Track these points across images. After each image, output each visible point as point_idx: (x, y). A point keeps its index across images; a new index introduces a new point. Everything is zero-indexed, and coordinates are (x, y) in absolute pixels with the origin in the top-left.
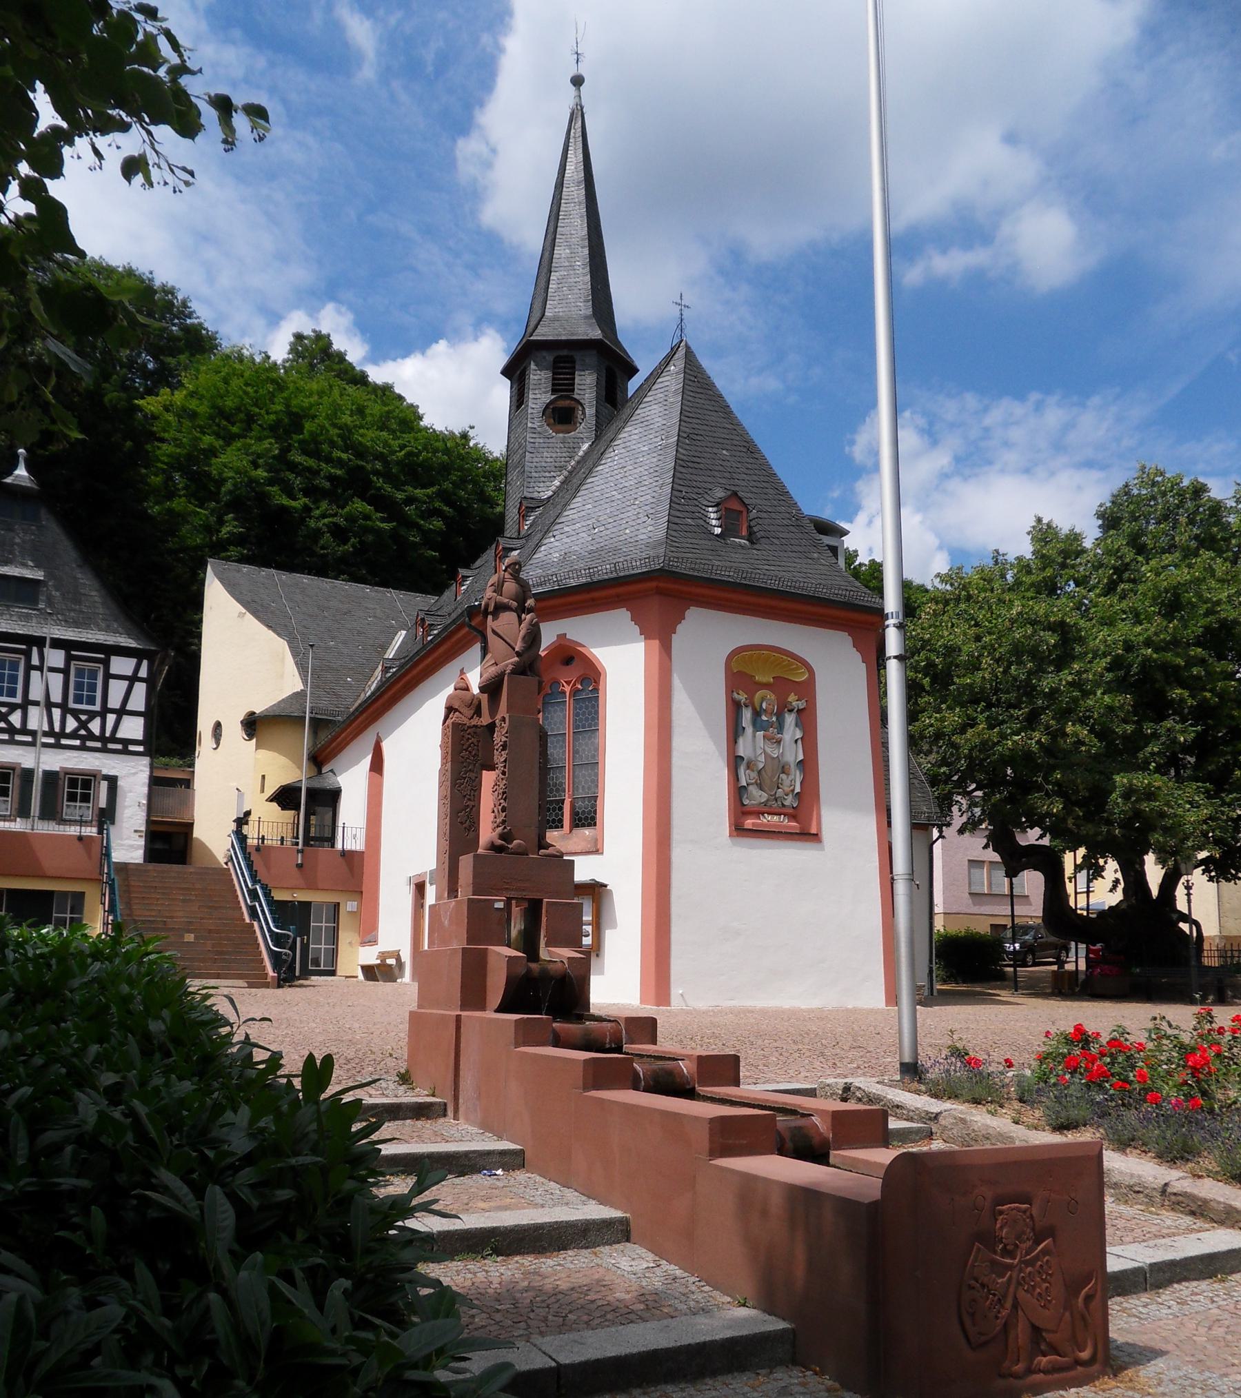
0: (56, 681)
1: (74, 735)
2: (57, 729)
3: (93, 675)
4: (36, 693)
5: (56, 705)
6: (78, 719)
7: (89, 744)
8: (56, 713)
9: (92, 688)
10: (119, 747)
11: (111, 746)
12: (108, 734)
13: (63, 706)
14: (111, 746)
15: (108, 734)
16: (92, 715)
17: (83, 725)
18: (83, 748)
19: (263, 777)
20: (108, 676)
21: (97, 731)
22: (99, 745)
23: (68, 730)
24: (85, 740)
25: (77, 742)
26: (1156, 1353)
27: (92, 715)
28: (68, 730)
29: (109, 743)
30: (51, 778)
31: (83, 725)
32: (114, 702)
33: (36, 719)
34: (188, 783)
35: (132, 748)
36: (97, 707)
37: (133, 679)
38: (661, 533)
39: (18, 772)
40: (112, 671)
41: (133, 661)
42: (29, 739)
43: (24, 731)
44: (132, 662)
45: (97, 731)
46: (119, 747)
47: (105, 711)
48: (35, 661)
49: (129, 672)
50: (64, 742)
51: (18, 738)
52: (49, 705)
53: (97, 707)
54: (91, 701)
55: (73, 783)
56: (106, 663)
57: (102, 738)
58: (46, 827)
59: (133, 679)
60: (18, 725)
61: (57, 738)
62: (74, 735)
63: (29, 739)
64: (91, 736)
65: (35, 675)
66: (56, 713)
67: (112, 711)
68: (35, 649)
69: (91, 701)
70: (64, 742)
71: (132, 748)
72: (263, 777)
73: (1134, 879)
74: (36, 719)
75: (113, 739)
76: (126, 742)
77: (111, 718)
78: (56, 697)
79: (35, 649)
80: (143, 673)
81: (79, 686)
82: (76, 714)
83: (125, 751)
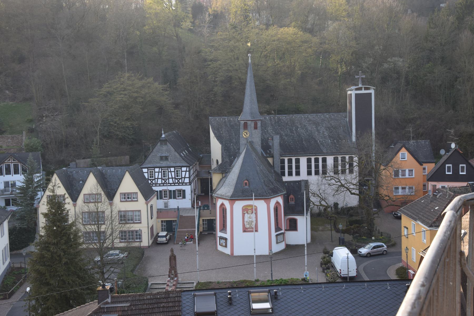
0: (173, 173)
1: (177, 183)
4: (170, 176)
9: (153, 174)
13: (175, 179)
17: (178, 181)
18: (179, 185)
20: (182, 171)
24: (179, 184)
26: (153, 225)
29: (183, 184)
31: (178, 181)
32: (156, 177)
33: (171, 181)
37: (186, 171)
47: (182, 178)
52: (172, 178)
54: (153, 177)
55: (165, 192)
57: (182, 183)
58: (465, 244)
59: (186, 171)
61: (174, 184)
62: (177, 183)
64: (180, 183)
65: (170, 173)
66: (174, 179)
73: (29, 181)
75: (184, 183)
76: (186, 183)
77: (183, 179)
78: (173, 177)
80: (188, 170)
81: (150, 175)
82: (177, 179)
83: (186, 185)
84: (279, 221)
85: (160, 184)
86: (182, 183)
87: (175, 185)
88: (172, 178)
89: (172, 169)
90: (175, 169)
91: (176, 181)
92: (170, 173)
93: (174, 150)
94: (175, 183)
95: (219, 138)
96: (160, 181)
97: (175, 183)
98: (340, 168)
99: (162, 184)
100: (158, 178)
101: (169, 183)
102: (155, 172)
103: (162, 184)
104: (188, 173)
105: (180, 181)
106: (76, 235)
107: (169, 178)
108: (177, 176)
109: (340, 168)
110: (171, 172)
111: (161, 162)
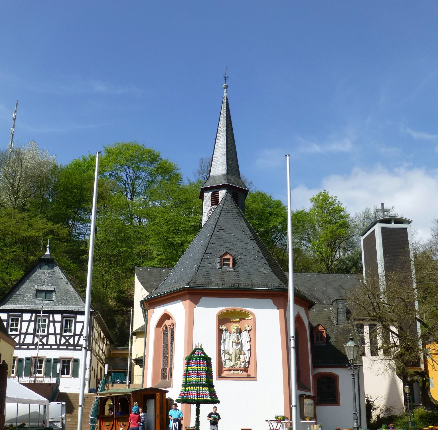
0: (58, 325)
1: (64, 345)
2: (58, 343)
3: (17, 320)
4: (52, 331)
5: (58, 334)
6: (65, 339)
7: (69, 348)
8: (58, 337)
10: (49, 347)
11: (77, 348)
12: (76, 343)
13: (61, 335)
14: (77, 348)
15: (76, 343)
16: (43, 336)
17: (67, 341)
18: (67, 349)
19: (137, 354)
20: (22, 321)
21: (72, 342)
22: (72, 348)
23: (62, 343)
24: (67, 346)
25: (65, 347)
27: (70, 337)
28: (62, 343)
29: (76, 347)
30: (28, 360)
31: (67, 341)
32: (24, 331)
33: (52, 340)
34: (362, 366)
35: (53, 347)
36: (72, 334)
38: (225, 172)
39: (45, 359)
40: (77, 320)
41: (30, 315)
42: (80, 348)
43: (47, 344)
44: (29, 315)
45: (72, 342)
46: (26, 347)
47: (21, 333)
48: (51, 319)
49: (28, 319)
50: (61, 347)
51: (45, 347)
53: (72, 334)
54: (70, 331)
56: (21, 316)
57: (19, 344)
59: (30, 321)
60: (45, 343)
61: (58, 346)
62: (64, 345)
63: (80, 348)
64: (70, 345)
66: (58, 337)
67: (77, 335)
68: (51, 315)
69: (16, 330)
70: (61, 347)
71: (53, 347)
72: (137, 354)
74: (52, 340)
78: (58, 331)
79: (51, 315)
80: (33, 319)
82: (65, 337)
83: (51, 349)
84: (354, 386)
85: (29, 345)
86: (74, 345)
87: (58, 349)
88: (55, 334)
89: (58, 317)
90: (63, 318)
91: (63, 340)
92: (51, 324)
93: (65, 280)
94: (60, 345)
95: (137, 275)
96: (29, 339)
97: (60, 345)
98: (380, 343)
99: (33, 344)
100: (26, 333)
101: (47, 344)
102: (76, 322)
103: (33, 344)
104: (32, 324)
105: (71, 341)
106: (388, 416)
107: (48, 334)
108: (66, 332)
109: (380, 343)
110: (54, 322)
111: (37, 302)
